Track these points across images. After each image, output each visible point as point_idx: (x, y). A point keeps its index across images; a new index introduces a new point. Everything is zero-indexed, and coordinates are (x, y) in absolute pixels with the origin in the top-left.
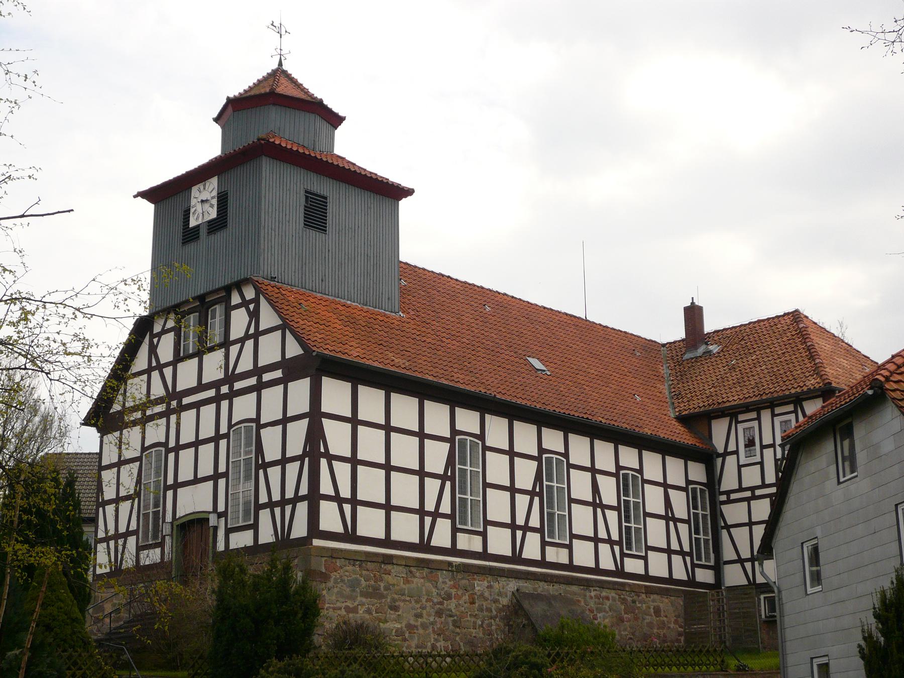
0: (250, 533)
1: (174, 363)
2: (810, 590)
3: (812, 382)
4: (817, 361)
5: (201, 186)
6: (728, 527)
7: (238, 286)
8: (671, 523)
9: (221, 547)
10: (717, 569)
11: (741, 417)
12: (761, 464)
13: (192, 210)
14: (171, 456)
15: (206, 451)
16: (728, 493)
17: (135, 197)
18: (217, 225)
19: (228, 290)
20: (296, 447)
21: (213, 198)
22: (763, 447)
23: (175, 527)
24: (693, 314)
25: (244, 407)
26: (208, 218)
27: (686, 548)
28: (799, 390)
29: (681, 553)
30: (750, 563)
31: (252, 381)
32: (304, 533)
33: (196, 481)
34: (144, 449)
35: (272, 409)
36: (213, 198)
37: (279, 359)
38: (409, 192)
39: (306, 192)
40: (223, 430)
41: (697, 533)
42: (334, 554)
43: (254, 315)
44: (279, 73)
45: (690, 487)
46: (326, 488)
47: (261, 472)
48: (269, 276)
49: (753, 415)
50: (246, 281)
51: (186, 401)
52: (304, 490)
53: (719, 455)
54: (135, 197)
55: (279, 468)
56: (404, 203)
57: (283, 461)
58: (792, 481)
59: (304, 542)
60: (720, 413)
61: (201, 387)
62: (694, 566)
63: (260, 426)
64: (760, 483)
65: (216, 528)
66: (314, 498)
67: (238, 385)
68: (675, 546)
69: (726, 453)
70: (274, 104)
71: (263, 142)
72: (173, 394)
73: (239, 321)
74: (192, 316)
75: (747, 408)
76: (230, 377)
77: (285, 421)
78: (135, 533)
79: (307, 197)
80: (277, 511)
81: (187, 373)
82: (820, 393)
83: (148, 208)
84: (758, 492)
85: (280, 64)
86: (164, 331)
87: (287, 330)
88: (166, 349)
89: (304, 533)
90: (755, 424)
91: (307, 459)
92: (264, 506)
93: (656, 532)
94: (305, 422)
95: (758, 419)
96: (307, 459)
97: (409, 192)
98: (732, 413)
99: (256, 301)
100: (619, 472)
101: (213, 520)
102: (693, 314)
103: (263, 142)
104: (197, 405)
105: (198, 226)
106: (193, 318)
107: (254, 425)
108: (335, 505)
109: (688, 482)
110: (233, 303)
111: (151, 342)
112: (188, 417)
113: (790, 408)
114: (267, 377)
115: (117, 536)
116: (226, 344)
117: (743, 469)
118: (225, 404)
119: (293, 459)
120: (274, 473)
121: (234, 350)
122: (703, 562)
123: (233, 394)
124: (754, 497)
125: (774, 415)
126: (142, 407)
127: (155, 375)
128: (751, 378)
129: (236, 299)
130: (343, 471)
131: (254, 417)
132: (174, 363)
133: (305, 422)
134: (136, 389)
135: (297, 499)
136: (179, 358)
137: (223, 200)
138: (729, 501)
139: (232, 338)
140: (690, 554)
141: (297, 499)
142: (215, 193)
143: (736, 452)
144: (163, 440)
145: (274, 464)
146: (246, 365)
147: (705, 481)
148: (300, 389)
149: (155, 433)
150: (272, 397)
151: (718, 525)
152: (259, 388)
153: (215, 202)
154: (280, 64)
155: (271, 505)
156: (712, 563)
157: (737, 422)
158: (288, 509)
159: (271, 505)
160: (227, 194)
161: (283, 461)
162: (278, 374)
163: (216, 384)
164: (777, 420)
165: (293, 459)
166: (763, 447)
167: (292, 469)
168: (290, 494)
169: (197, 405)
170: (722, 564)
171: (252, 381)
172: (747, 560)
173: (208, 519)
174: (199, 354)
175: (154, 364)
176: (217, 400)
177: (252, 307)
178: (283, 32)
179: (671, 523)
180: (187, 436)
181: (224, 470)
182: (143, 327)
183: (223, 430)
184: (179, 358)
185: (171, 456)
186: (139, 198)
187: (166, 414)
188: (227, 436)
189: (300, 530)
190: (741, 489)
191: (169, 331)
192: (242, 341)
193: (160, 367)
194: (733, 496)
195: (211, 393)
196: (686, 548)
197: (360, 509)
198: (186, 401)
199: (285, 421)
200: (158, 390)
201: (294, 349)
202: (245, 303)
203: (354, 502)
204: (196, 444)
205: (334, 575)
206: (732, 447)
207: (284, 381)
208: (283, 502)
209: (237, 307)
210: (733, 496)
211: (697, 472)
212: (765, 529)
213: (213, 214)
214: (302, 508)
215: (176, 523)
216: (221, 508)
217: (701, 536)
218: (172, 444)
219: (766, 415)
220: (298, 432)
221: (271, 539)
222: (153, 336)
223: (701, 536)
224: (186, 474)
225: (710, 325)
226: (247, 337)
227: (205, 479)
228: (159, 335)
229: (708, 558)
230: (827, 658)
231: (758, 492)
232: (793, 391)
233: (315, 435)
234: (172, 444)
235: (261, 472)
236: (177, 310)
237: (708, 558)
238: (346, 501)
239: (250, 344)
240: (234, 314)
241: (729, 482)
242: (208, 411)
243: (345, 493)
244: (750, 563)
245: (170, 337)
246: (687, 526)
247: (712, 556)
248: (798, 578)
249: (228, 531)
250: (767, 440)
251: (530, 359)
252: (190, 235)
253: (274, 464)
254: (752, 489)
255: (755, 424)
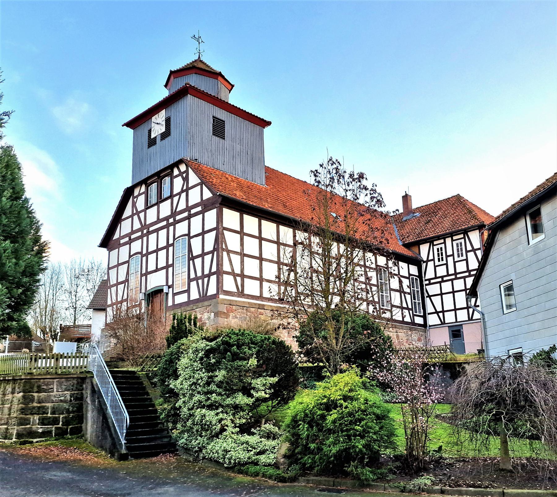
0: (186, 295)
1: (145, 210)
2: (505, 312)
3: (473, 223)
4: (474, 213)
5: (157, 116)
6: (429, 296)
7: (177, 164)
8: (402, 294)
9: (170, 303)
10: (424, 317)
11: (435, 243)
12: (447, 264)
13: (152, 129)
14: (144, 258)
15: (162, 254)
16: (429, 280)
17: (123, 126)
18: (165, 135)
19: (171, 167)
20: (209, 246)
21: (163, 121)
22: (447, 256)
23: (146, 295)
24: (406, 198)
25: (181, 228)
26: (160, 132)
27: (410, 307)
28: (466, 226)
29: (407, 308)
30: (442, 313)
31: (186, 214)
32: (215, 292)
33: (157, 270)
34: (130, 256)
35: (196, 228)
36: (163, 121)
37: (200, 201)
38: (269, 123)
39: (213, 117)
40: (171, 241)
41: (415, 299)
42: (231, 303)
43: (186, 180)
44: (199, 60)
45: (411, 277)
46: (226, 267)
47: (191, 262)
48: (193, 158)
49: (442, 241)
50: (181, 161)
51: (151, 229)
52: (214, 269)
53: (424, 262)
54: (123, 126)
55: (200, 259)
56: (267, 130)
57: (203, 255)
58: (492, 251)
59: (215, 296)
60: (424, 241)
61: (159, 221)
62: (414, 315)
63: (190, 238)
64: (446, 274)
65: (167, 294)
66: (219, 273)
67: (178, 218)
68: (404, 305)
69: (428, 261)
70: (196, 73)
71: (188, 86)
72: (145, 226)
73: (178, 183)
74: (154, 184)
75: (438, 238)
76: (174, 214)
77: (204, 233)
78: (126, 300)
79: (214, 120)
80: (200, 281)
81: (152, 215)
82: (477, 228)
83: (130, 132)
84: (445, 279)
85: (199, 57)
86: (140, 194)
87: (203, 185)
88: (141, 203)
89: (215, 292)
90: (443, 246)
91: (215, 253)
92: (193, 280)
93: (396, 298)
94: (214, 232)
95: (445, 243)
96: (215, 253)
97: (269, 123)
98: (430, 241)
99: (187, 172)
100: (378, 269)
101: (165, 290)
102: (406, 198)
103: (188, 86)
104: (157, 231)
105: (156, 137)
106: (154, 185)
107: (187, 237)
108: (231, 277)
109: (410, 275)
110: (174, 175)
111: (133, 201)
112: (152, 237)
113: (462, 236)
114: (193, 211)
115: (117, 303)
116: (171, 197)
117: (437, 268)
118: (171, 228)
119: (208, 253)
120: (198, 261)
121: (176, 199)
122: (418, 314)
123: (176, 222)
124: (443, 281)
125: (452, 240)
126: (129, 235)
127: (136, 217)
128: (439, 224)
129: (176, 172)
130: (236, 259)
131: (187, 233)
132: (145, 210)
133: (214, 232)
134: (125, 227)
135: (211, 274)
136: (148, 207)
137: (168, 121)
138: (430, 284)
139: (174, 193)
140: (412, 309)
141: (211, 274)
142: (164, 118)
143: (433, 260)
144: (140, 251)
145: (198, 257)
146: (182, 206)
147: (418, 275)
148: (211, 216)
149: (136, 246)
150: (196, 222)
151: (423, 295)
152: (189, 218)
153: (164, 123)
154: (199, 57)
155: (196, 279)
156: (422, 314)
157: (433, 245)
158: (206, 280)
159: (196, 279)
160: (170, 118)
161: (203, 255)
162: (199, 209)
163: (167, 219)
164: (455, 243)
165: (208, 253)
166: (447, 256)
167: (208, 258)
168: (206, 272)
169: (157, 231)
170: (427, 314)
171: (186, 214)
172: (440, 312)
173: (163, 289)
174: (157, 204)
175: (135, 212)
176: (167, 227)
177: (184, 175)
178: (200, 42)
179: (402, 294)
180: (152, 247)
181: (172, 263)
182: (128, 193)
183: (171, 241)
184: (148, 207)
185: (144, 258)
186: (125, 126)
187: (141, 237)
188: (173, 245)
189: (212, 290)
190: (436, 278)
191: (142, 194)
192: (179, 194)
193: (138, 213)
194: (432, 281)
195: (164, 223)
196: (410, 307)
197: (246, 280)
198: (151, 229)
199: (204, 233)
200: (137, 226)
201: (207, 194)
202: (181, 174)
203: (243, 276)
204: (157, 251)
205: (231, 315)
206: (431, 257)
207: (202, 212)
208: (203, 276)
209: (177, 176)
210: (432, 281)
211: (414, 270)
212: (473, 281)
213: (163, 130)
214: (213, 278)
215: (147, 293)
216: (170, 283)
217: (416, 301)
218: (144, 252)
219: (449, 241)
220: (210, 238)
221: (198, 297)
222: (134, 198)
223: (416, 301)
224: (151, 267)
225: (415, 204)
226: (182, 191)
227: (162, 268)
228: (137, 197)
229: (420, 312)
230: (521, 349)
231: (445, 279)
232: (463, 227)
233: (219, 241)
234: (144, 252)
235: (191, 262)
236: (146, 182)
237: (420, 312)
238: (238, 275)
239: (184, 195)
240: (175, 180)
241: (430, 274)
242: (163, 233)
243: (238, 271)
244: (442, 313)
245: (143, 197)
246: (410, 296)
247: (422, 310)
248: (498, 305)
249: (174, 295)
250: (449, 252)
251: (332, 213)
252: (152, 142)
253: (198, 257)
254: (442, 277)
255: (443, 246)
